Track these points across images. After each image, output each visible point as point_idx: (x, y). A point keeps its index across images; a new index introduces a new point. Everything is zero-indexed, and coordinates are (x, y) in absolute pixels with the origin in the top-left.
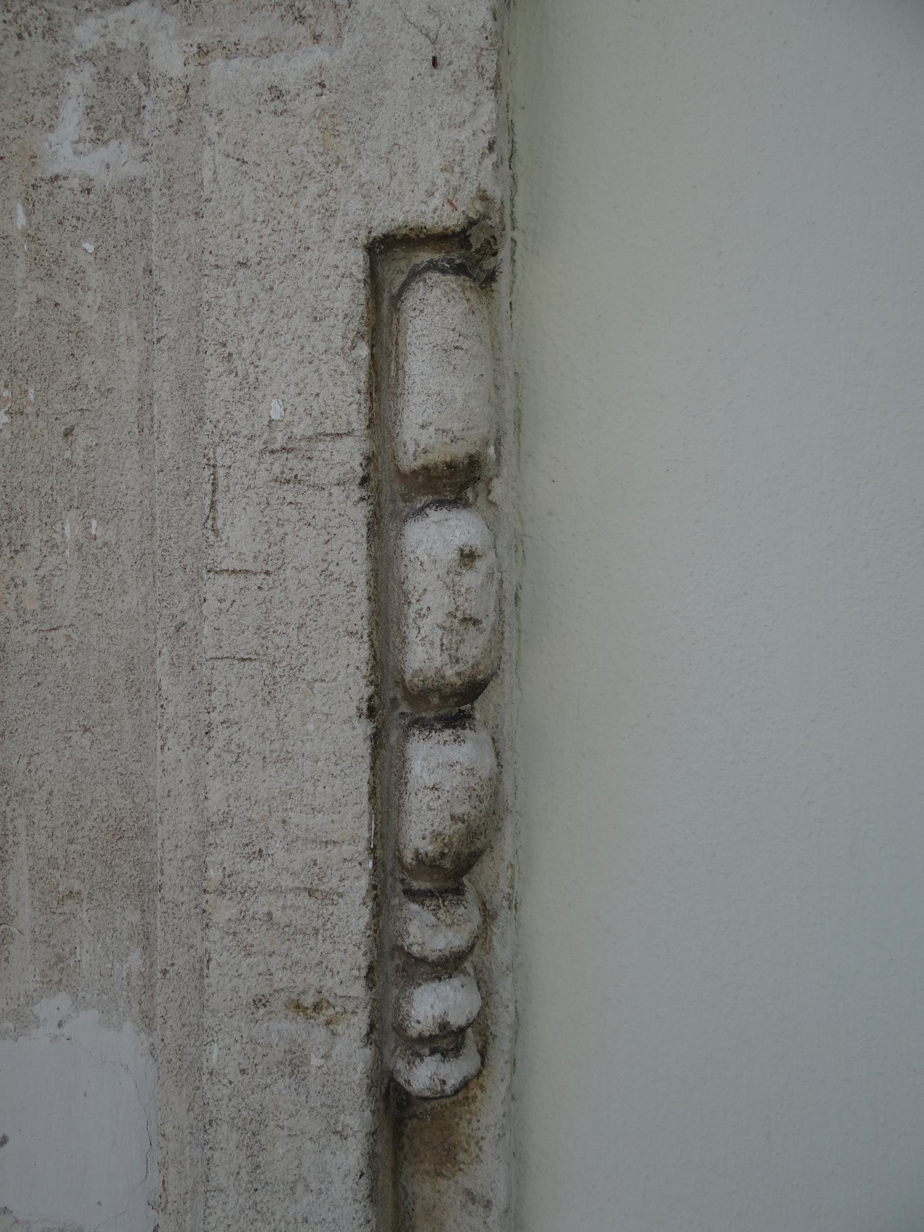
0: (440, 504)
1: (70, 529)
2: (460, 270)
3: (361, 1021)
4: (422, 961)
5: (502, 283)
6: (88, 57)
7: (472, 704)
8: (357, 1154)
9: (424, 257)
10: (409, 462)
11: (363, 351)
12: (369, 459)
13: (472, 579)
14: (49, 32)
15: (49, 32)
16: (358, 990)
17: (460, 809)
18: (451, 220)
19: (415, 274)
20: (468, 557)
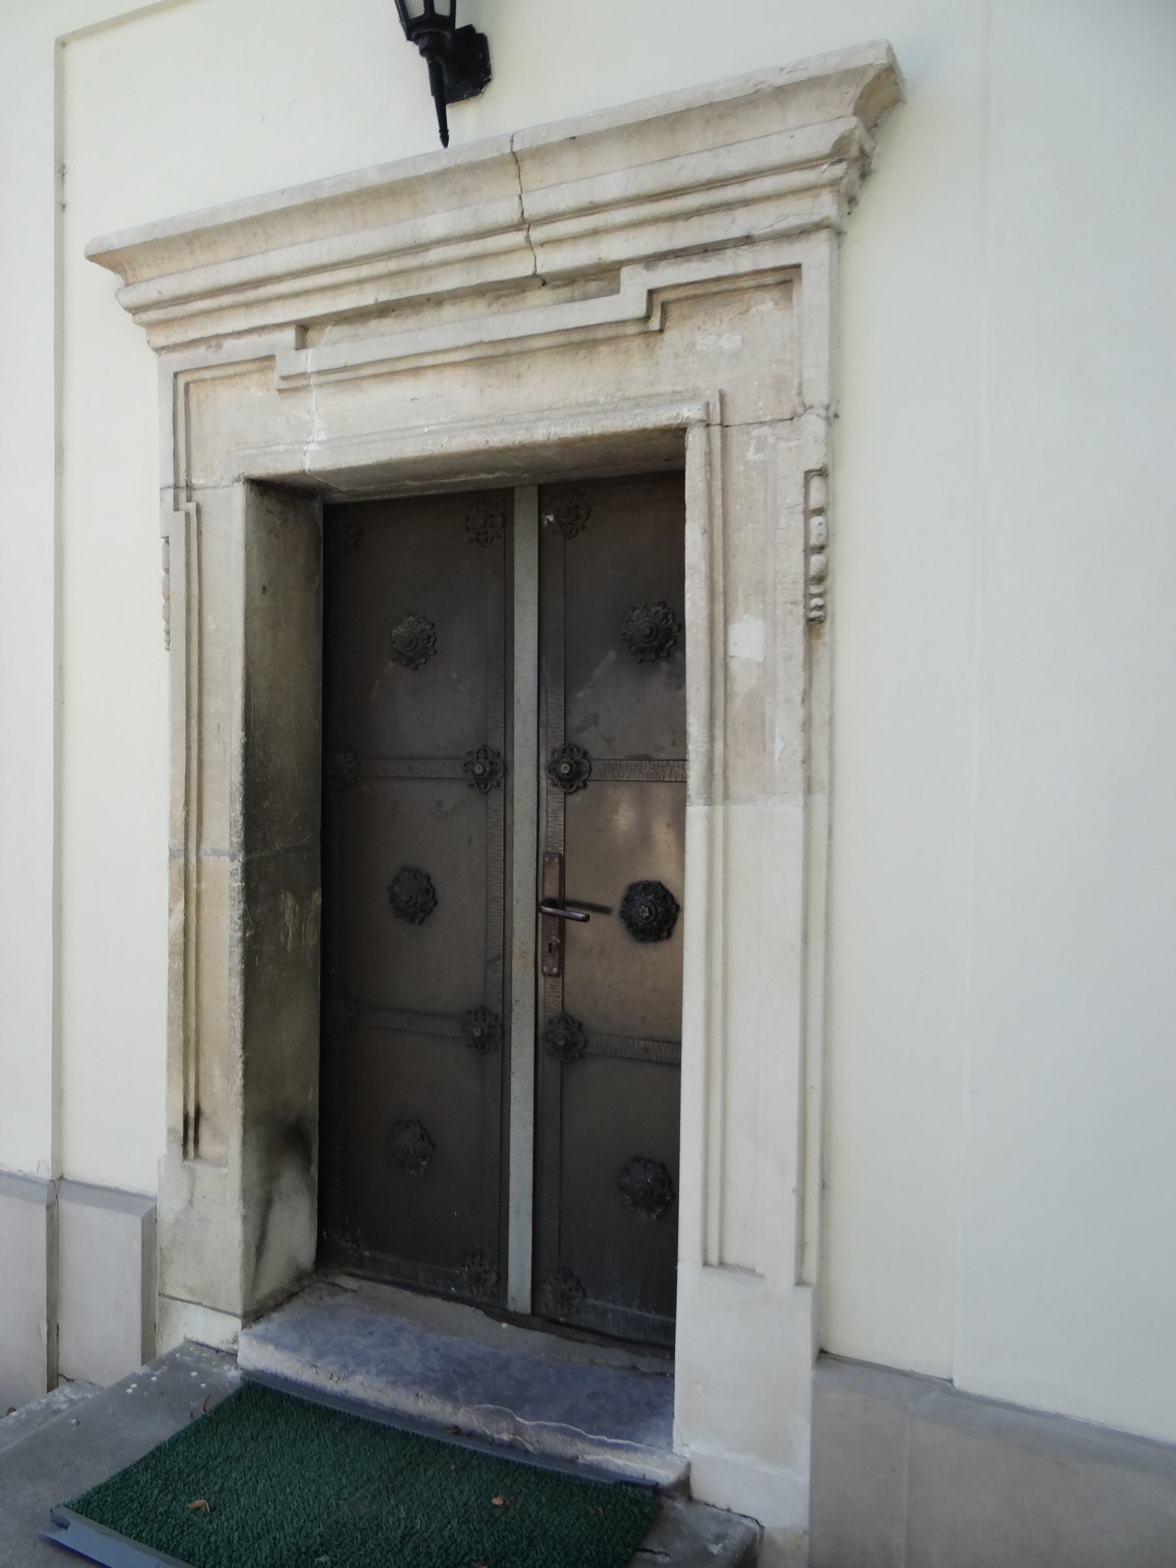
0: (816, 515)
1: (750, 526)
2: (820, 475)
3: (802, 605)
4: (812, 595)
5: (830, 476)
6: (755, 437)
7: (547, 850)
8: (405, 1292)
9: (814, 473)
10: (811, 508)
11: (803, 490)
12: (804, 508)
13: (822, 527)
14: (748, 433)
15: (748, 433)
16: (802, 599)
17: (818, 567)
18: (818, 467)
19: (813, 476)
20: (821, 524)
